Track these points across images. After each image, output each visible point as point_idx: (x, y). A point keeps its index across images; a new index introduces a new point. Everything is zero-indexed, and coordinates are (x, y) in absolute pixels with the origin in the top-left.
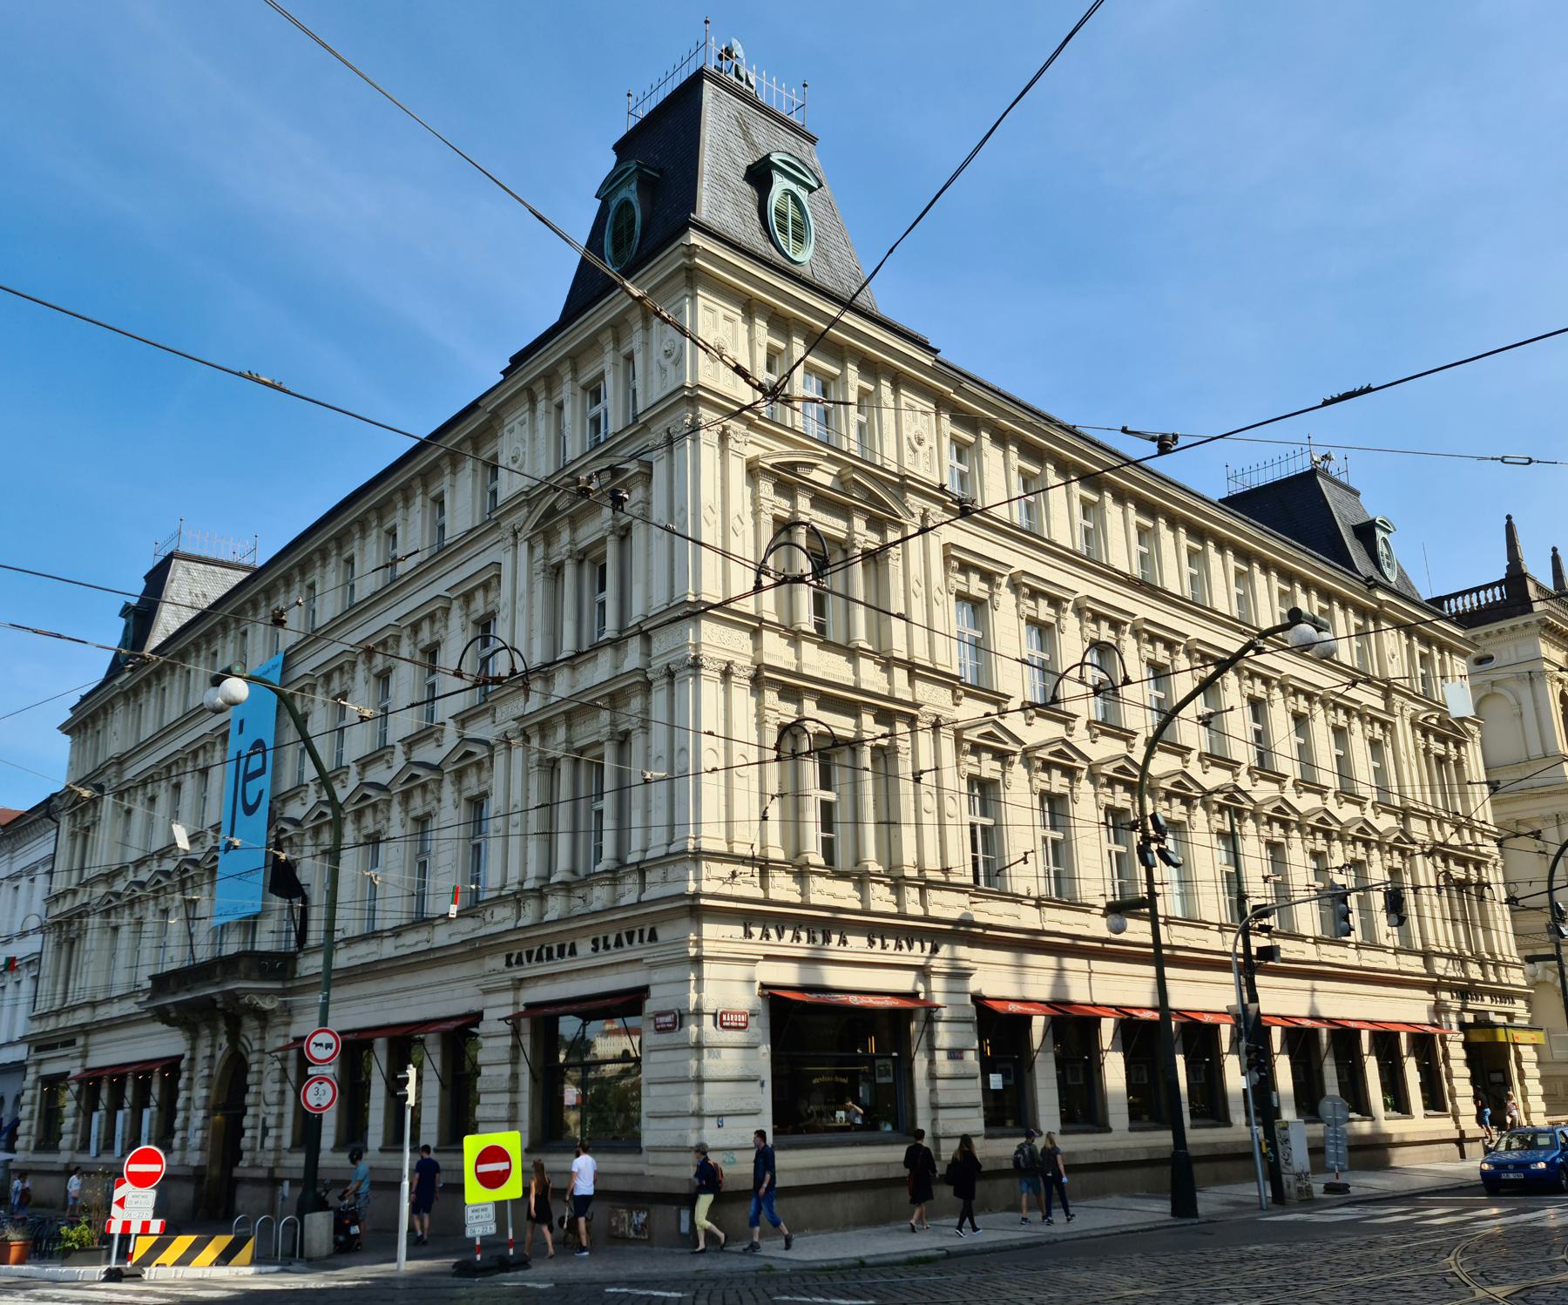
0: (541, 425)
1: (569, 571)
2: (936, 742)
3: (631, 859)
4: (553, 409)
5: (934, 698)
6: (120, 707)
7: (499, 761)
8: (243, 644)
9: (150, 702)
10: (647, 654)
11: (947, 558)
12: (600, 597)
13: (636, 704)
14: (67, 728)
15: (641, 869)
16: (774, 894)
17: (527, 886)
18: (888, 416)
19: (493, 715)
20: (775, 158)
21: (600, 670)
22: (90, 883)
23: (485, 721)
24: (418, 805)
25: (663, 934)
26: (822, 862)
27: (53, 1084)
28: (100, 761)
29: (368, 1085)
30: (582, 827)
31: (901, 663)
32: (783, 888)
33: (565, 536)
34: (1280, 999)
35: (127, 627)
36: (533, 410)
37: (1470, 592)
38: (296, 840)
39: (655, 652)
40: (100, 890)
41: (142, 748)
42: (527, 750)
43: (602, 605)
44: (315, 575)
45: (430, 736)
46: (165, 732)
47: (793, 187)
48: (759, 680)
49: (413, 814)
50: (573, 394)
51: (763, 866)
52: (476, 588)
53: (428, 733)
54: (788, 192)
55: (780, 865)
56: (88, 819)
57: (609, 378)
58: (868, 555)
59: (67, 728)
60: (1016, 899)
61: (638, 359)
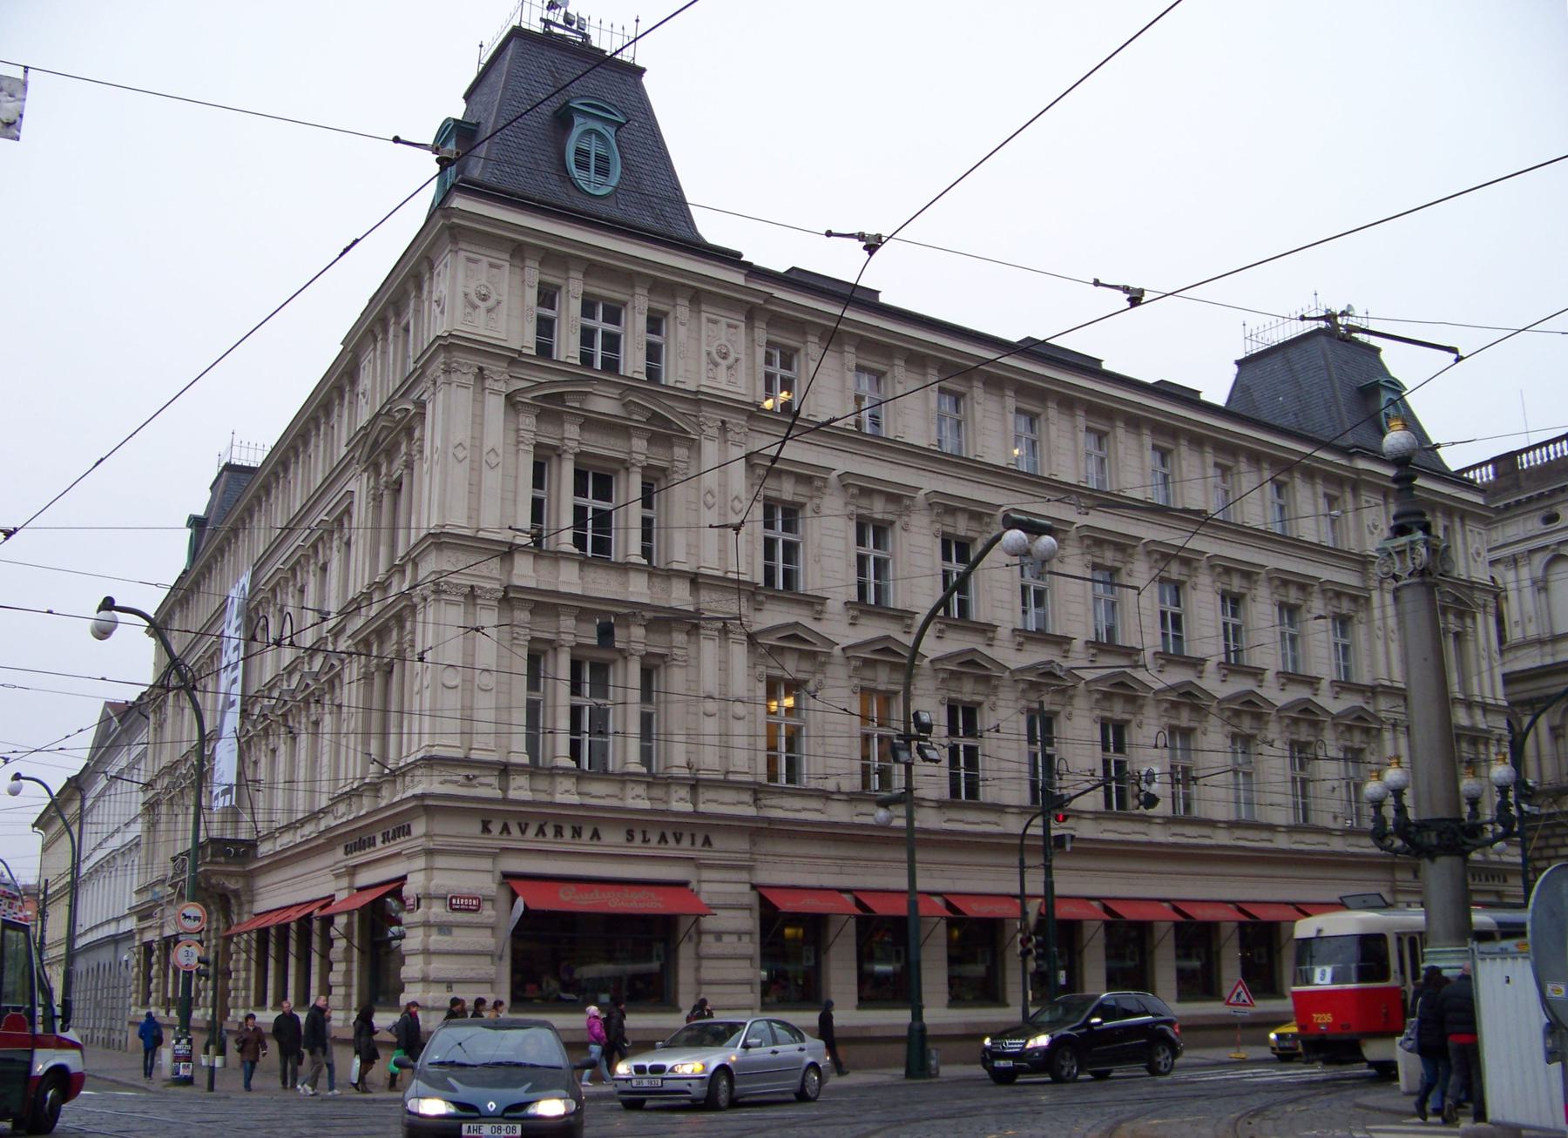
2: (1395, 739)
16: (512, 794)
18: (1459, 538)
25: (717, 842)
26: (525, 759)
27: (148, 947)
31: (681, 574)
32: (520, 789)
34: (1079, 883)
37: (1540, 445)
47: (598, 126)
48: (508, 598)
51: (505, 770)
55: (520, 769)
58: (1457, 635)
60: (1211, 823)
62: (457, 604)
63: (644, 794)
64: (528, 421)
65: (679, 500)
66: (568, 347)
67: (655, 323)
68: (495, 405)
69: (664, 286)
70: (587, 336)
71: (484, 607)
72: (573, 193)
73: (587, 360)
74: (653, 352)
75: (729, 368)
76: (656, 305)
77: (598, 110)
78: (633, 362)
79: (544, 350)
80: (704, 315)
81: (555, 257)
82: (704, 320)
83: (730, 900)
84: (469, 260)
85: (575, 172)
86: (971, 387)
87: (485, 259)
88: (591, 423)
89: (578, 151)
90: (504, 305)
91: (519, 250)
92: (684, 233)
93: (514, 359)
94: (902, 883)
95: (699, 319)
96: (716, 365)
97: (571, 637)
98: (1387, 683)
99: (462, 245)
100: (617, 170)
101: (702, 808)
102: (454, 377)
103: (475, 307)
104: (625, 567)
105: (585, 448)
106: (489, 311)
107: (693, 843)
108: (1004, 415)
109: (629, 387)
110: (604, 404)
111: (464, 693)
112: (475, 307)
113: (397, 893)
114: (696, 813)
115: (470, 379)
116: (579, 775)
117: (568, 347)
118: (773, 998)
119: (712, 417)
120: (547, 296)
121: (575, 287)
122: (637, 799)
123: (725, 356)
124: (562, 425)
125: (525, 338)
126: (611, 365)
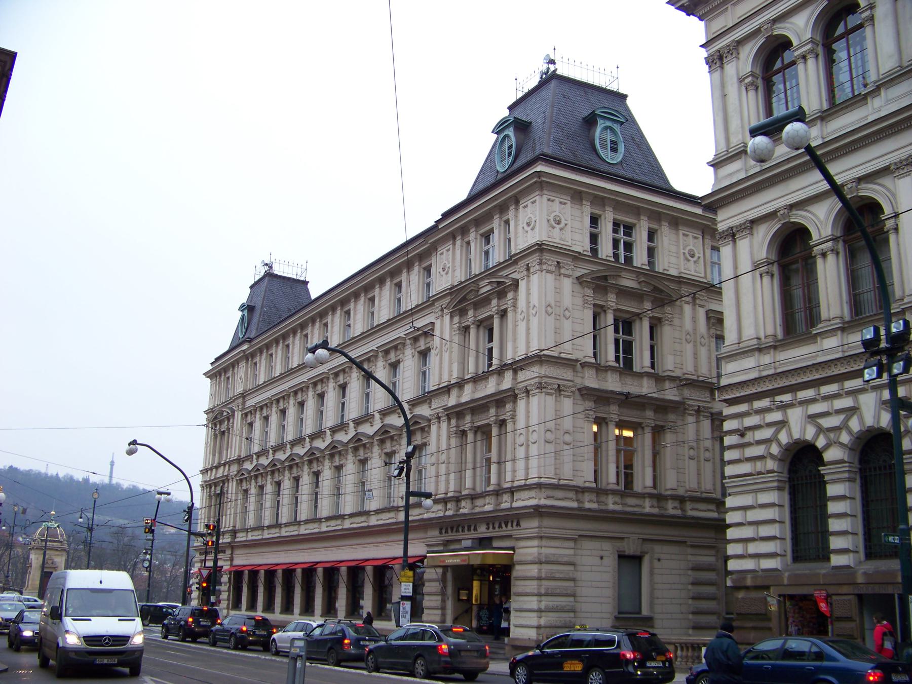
0: (458, 252)
1: (473, 331)
3: (506, 485)
4: (502, 223)
5: (695, 397)
6: (243, 364)
7: (434, 428)
8: (228, 383)
9: (262, 362)
10: (515, 379)
11: (708, 318)
12: (490, 345)
13: (509, 406)
14: (210, 375)
15: (512, 491)
17: (450, 495)
19: (430, 403)
20: (597, 112)
21: (490, 387)
22: (229, 463)
23: (368, 425)
24: (315, 468)
28: (231, 395)
29: (314, 587)
30: (478, 465)
33: (471, 313)
35: (243, 316)
36: (454, 244)
38: (321, 459)
39: (519, 379)
40: (234, 468)
41: (259, 388)
42: (449, 424)
43: (490, 350)
44: (290, 341)
45: (319, 436)
46: (272, 381)
47: (609, 124)
48: (586, 393)
49: (385, 451)
50: (500, 225)
52: (318, 381)
53: (366, 418)
54: (607, 128)
56: (224, 427)
57: (496, 231)
59: (210, 375)
61: (512, 223)
62: (551, 394)
63: (595, 499)
64: (589, 292)
65: (667, 333)
66: (606, 250)
67: (651, 235)
68: (567, 284)
69: (657, 215)
70: (616, 243)
71: (565, 396)
72: (594, 157)
73: (616, 256)
74: (651, 252)
75: (695, 262)
76: (651, 226)
77: (611, 116)
78: (640, 258)
79: (594, 251)
80: (681, 232)
81: (600, 200)
82: (681, 236)
83: (529, 558)
84: (549, 200)
85: (601, 152)
86: (660, 226)
87: (557, 200)
88: (623, 293)
89: (600, 139)
90: (569, 226)
91: (577, 195)
92: (657, 183)
93: (576, 257)
94: (399, 552)
95: (677, 234)
96: (689, 261)
97: (616, 417)
98: (695, 378)
99: (545, 192)
100: (622, 149)
101: (515, 505)
102: (544, 267)
103: (554, 228)
104: (641, 375)
105: (620, 307)
106: (561, 229)
107: (512, 526)
108: (582, 217)
109: (639, 272)
110: (628, 282)
111: (545, 444)
112: (554, 228)
113: (422, 561)
114: (511, 509)
115: (553, 268)
116: (622, 494)
117: (606, 250)
118: (137, 655)
119: (685, 290)
120: (594, 220)
121: (608, 218)
122: (648, 507)
123: (559, 223)
124: (643, 302)
125: (582, 245)
126: (629, 260)
